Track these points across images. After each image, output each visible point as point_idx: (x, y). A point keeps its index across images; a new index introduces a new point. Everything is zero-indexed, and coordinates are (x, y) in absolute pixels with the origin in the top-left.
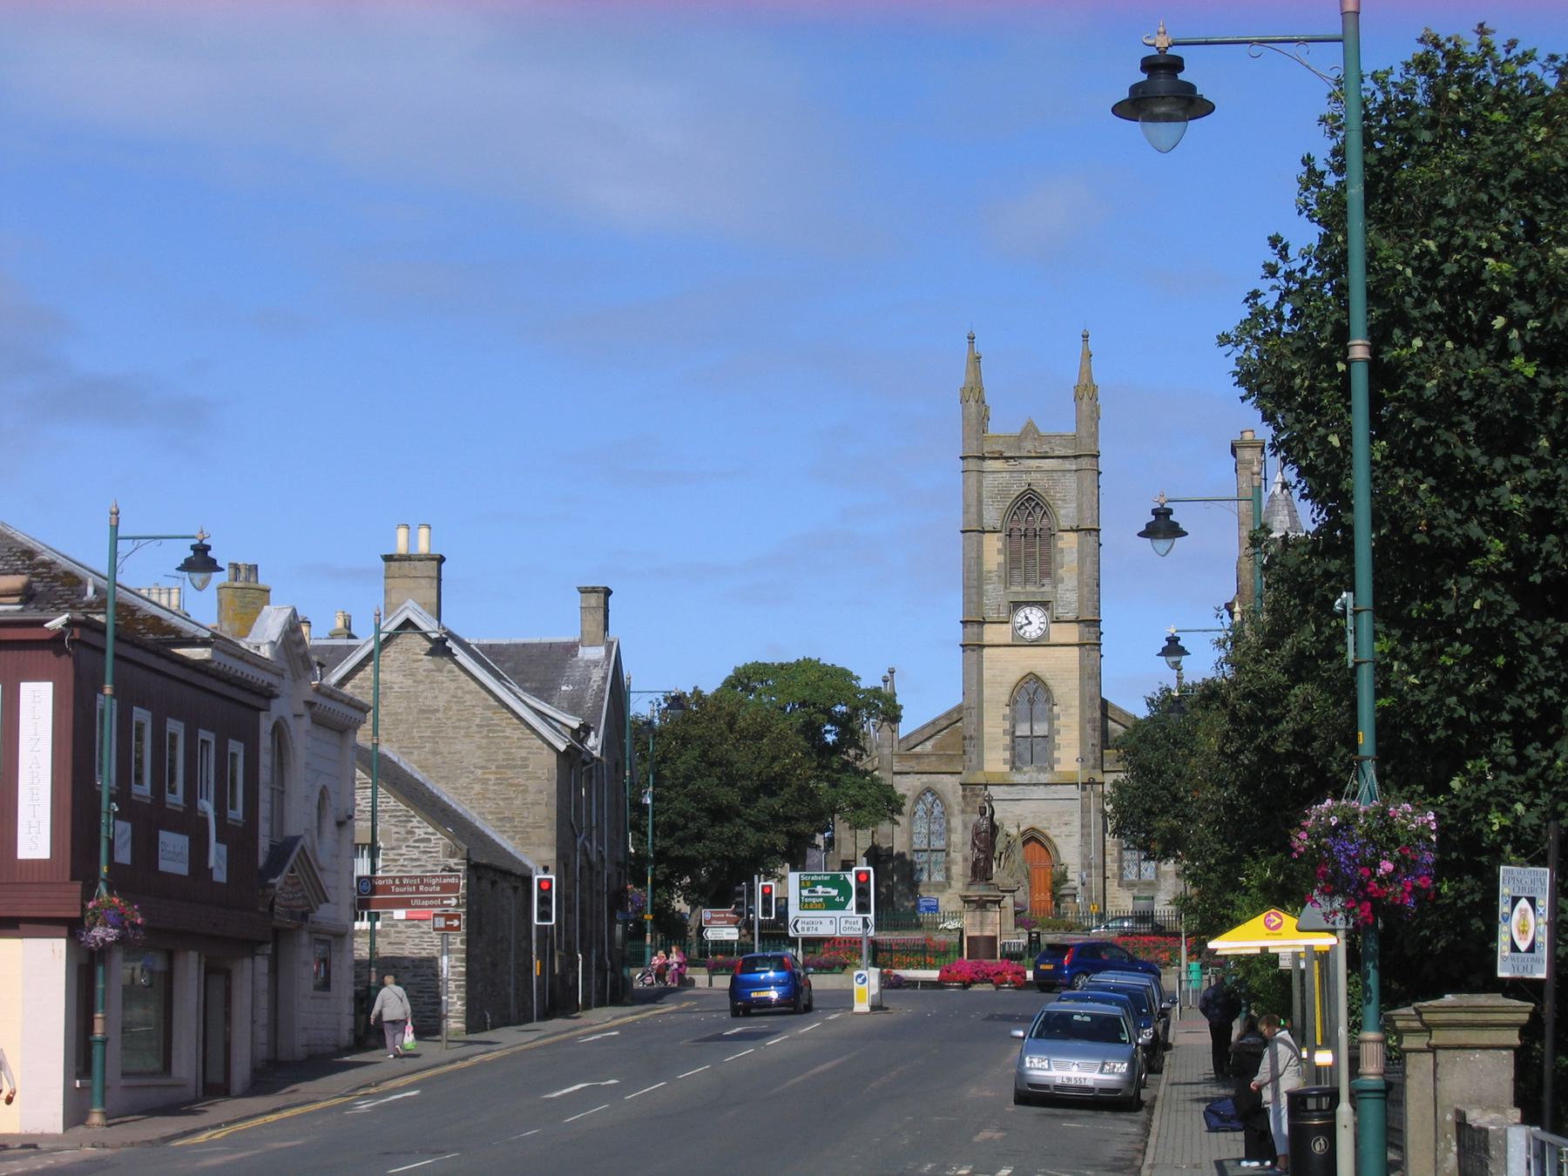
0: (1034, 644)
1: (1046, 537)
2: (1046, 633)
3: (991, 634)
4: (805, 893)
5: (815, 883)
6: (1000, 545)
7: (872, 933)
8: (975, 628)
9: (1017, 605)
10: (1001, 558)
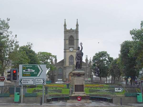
0: (72, 52)
1: (73, 40)
2: (73, 51)
3: (67, 51)
4: (24, 71)
5: (28, 68)
6: (68, 41)
7: (45, 84)
8: (65, 50)
9: (70, 48)
10: (68, 43)
